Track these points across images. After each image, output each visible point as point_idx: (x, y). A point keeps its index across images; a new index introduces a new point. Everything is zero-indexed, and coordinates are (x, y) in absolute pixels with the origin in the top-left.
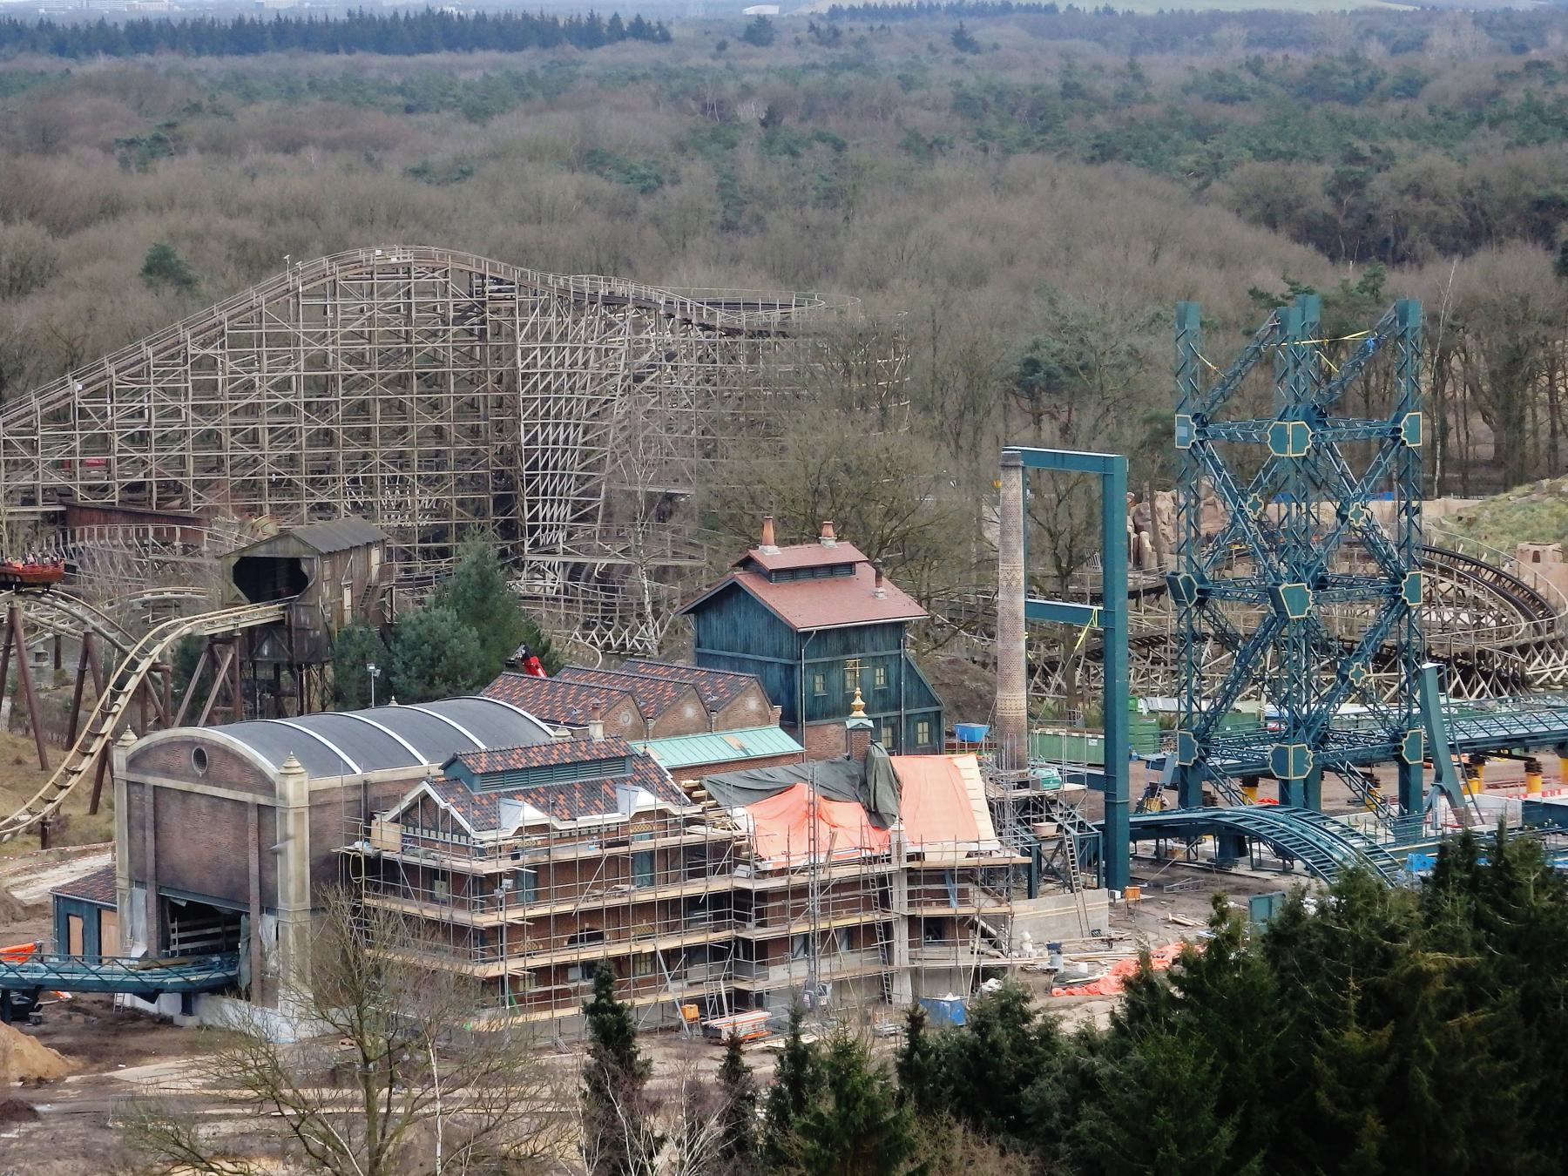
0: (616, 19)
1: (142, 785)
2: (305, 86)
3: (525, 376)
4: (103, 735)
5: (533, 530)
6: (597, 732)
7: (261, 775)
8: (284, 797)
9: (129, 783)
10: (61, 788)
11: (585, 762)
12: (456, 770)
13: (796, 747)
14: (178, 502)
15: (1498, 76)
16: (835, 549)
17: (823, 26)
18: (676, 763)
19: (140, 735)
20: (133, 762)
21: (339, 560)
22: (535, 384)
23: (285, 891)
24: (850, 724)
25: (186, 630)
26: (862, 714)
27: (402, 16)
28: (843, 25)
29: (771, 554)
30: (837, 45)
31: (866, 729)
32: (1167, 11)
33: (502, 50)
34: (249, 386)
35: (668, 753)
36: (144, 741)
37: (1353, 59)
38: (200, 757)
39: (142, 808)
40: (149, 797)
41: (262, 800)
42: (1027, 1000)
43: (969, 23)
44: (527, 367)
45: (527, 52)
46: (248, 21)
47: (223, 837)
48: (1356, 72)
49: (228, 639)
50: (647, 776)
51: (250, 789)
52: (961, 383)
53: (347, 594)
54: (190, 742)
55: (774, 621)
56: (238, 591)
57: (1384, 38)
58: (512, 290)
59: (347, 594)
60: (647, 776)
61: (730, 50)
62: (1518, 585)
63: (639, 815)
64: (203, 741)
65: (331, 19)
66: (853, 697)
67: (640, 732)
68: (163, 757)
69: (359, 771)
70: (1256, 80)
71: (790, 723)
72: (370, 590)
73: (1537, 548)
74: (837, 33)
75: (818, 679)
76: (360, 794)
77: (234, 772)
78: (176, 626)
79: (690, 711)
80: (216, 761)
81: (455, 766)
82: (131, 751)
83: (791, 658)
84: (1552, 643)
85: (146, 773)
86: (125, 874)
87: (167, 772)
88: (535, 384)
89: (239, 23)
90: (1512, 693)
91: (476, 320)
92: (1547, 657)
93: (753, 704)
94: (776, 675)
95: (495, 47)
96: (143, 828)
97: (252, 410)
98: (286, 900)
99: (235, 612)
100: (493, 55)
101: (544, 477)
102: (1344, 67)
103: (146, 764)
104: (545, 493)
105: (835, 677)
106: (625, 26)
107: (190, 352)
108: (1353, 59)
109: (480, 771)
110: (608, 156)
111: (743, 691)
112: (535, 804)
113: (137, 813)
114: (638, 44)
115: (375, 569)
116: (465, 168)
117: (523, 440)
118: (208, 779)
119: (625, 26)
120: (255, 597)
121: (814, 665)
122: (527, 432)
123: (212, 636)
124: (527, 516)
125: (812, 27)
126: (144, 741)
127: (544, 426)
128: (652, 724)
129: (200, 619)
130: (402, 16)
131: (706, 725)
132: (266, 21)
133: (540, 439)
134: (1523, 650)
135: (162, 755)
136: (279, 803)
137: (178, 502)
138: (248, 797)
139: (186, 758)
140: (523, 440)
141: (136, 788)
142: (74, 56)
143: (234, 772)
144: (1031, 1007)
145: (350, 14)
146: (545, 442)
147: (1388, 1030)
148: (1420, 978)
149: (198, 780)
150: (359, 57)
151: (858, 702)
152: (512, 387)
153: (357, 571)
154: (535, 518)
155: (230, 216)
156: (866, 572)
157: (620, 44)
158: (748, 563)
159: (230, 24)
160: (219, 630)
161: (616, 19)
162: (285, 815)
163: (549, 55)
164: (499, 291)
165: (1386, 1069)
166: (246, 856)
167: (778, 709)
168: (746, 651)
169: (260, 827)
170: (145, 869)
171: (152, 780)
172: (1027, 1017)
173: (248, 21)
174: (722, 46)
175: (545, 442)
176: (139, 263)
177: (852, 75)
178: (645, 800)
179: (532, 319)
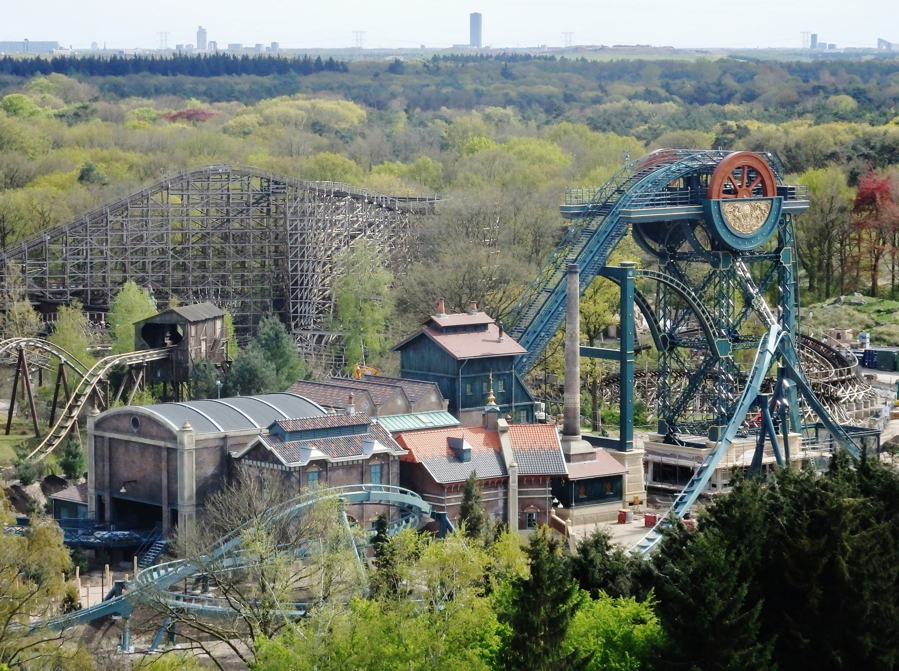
0: (319, 59)
1: (103, 437)
2: (153, 90)
3: (291, 234)
4: (73, 417)
5: (295, 318)
6: (352, 411)
7: (169, 431)
8: (182, 444)
9: (95, 436)
10: (56, 437)
11: (346, 427)
12: (275, 430)
13: (457, 422)
14: (101, 301)
15: (799, 93)
16: (480, 317)
17: (431, 65)
18: (393, 429)
19: (102, 411)
20: (98, 425)
21: (200, 326)
22: (296, 239)
23: (182, 495)
24: (487, 408)
25: (117, 362)
26: (493, 403)
27: (202, 57)
28: (442, 64)
29: (445, 319)
30: (438, 75)
31: (496, 411)
32: (614, 61)
33: (257, 75)
34: (141, 238)
35: (391, 424)
36: (105, 413)
37: (719, 84)
38: (135, 422)
39: (103, 451)
40: (106, 444)
41: (170, 445)
42: (609, 538)
43: (509, 64)
44: (292, 230)
45: (271, 76)
46: (118, 58)
47: (148, 465)
48: (720, 91)
49: (139, 367)
50: (381, 435)
51: (163, 439)
52: (530, 237)
53: (203, 344)
54: (129, 414)
55: (445, 354)
56: (144, 342)
57: (734, 75)
58: (284, 188)
59: (203, 344)
60: (381, 435)
61: (381, 76)
62: (829, 349)
63: (374, 456)
64: (137, 414)
65: (164, 57)
66: (489, 394)
67: (373, 413)
68: (115, 422)
69: (222, 430)
70: (667, 94)
71: (453, 410)
72: (216, 342)
73: (839, 331)
74: (438, 68)
75: (468, 386)
76: (220, 443)
77: (154, 430)
78: (112, 360)
79: (400, 402)
80: (144, 424)
81: (275, 427)
82: (96, 419)
83: (454, 374)
84: (849, 380)
85: (105, 430)
86: (93, 486)
87: (117, 430)
88: (296, 239)
89: (114, 59)
90: (830, 405)
91: (265, 204)
92: (846, 388)
93: (433, 398)
94: (446, 383)
95: (254, 73)
96: (103, 461)
97: (144, 251)
98: (182, 499)
99: (142, 352)
100: (253, 77)
101: (301, 289)
102: (714, 88)
103: (105, 426)
104: (301, 298)
105: (477, 385)
106: (324, 64)
107: (109, 219)
108: (719, 84)
109: (289, 430)
110: (324, 126)
111: (429, 392)
112: (319, 448)
113: (99, 453)
114: (331, 73)
115: (218, 331)
116: (246, 130)
117: (290, 270)
118: (140, 434)
119: (324, 64)
120: (153, 346)
121: (466, 378)
122: (292, 265)
123: (130, 366)
124: (292, 311)
125: (425, 65)
126: (105, 413)
127: (301, 262)
128: (379, 409)
129: (125, 356)
130: (202, 57)
131: (408, 410)
132: (128, 58)
133: (299, 269)
134: (834, 383)
135: (114, 421)
136: (179, 447)
137: (101, 301)
138: (162, 444)
139: (127, 423)
140: (290, 270)
141: (99, 439)
142: (24, 75)
143: (154, 430)
144: (610, 542)
145: (174, 54)
146: (302, 270)
147: (823, 541)
148: (840, 510)
149: (133, 434)
150: (180, 77)
151: (492, 397)
152: (284, 241)
153: (209, 331)
154: (296, 312)
155: (124, 151)
156: (493, 330)
157: (322, 72)
158: (430, 323)
159: (109, 60)
160: (134, 362)
161: (319, 59)
162: (182, 453)
163: (283, 78)
164: (277, 188)
165: (824, 561)
166: (160, 475)
167: (447, 402)
168: (429, 370)
169: (168, 461)
170: (103, 483)
171: (108, 435)
172: (609, 548)
173: (118, 58)
174: (377, 75)
175: (302, 270)
176: (76, 173)
177: (450, 89)
178: (379, 447)
179: (295, 205)
